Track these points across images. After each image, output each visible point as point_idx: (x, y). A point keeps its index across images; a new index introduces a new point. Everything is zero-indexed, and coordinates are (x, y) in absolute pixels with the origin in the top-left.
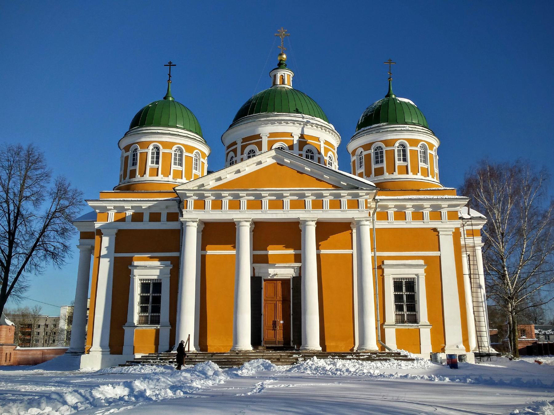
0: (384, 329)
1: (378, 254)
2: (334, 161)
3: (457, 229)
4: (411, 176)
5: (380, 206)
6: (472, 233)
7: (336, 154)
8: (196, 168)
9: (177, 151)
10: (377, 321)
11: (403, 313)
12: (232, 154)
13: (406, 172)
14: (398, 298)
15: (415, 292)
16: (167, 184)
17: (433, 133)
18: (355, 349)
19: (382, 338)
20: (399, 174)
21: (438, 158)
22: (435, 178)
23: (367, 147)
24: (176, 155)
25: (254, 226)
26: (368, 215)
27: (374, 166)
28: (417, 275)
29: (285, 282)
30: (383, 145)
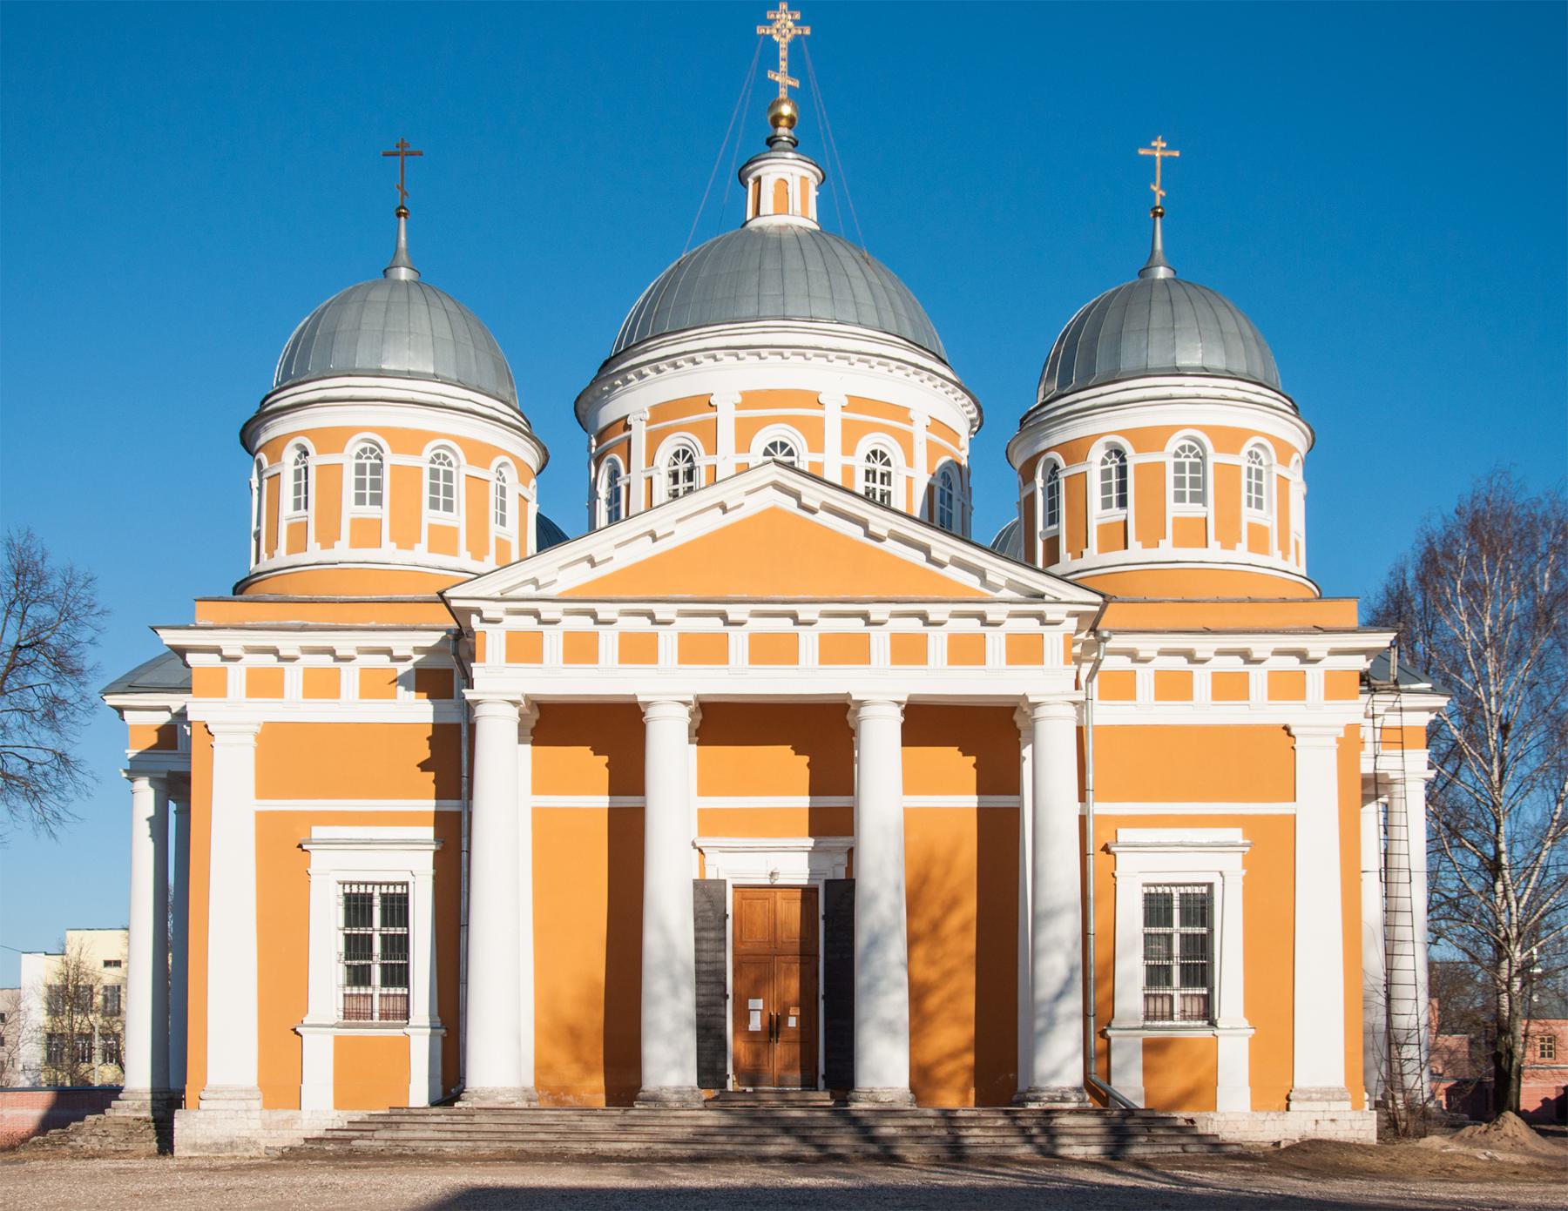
3: (1353, 729)
4: (1137, 552)
6: (1397, 739)
9: (438, 462)
17: (1294, 407)
20: (430, 550)
24: (1179, 468)
25: (700, 717)
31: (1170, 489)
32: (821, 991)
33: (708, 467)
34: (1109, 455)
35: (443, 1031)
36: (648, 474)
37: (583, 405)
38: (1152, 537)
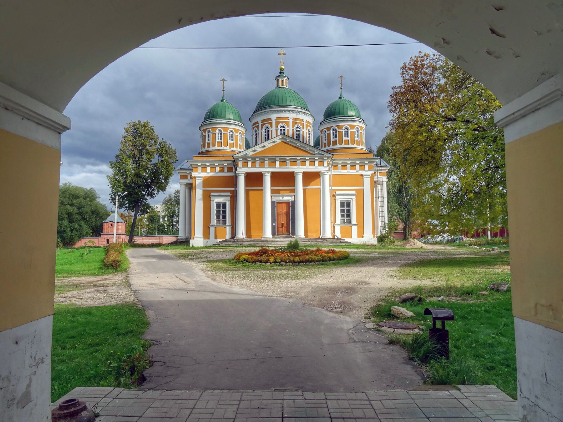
5: (335, 163)
6: (381, 174)
10: (331, 222)
11: (344, 218)
12: (256, 129)
14: (342, 211)
16: (226, 151)
18: (321, 236)
23: (329, 129)
24: (230, 134)
26: (328, 169)
28: (352, 199)
29: (287, 203)
30: (336, 128)
32: (290, 219)
38: (341, 143)
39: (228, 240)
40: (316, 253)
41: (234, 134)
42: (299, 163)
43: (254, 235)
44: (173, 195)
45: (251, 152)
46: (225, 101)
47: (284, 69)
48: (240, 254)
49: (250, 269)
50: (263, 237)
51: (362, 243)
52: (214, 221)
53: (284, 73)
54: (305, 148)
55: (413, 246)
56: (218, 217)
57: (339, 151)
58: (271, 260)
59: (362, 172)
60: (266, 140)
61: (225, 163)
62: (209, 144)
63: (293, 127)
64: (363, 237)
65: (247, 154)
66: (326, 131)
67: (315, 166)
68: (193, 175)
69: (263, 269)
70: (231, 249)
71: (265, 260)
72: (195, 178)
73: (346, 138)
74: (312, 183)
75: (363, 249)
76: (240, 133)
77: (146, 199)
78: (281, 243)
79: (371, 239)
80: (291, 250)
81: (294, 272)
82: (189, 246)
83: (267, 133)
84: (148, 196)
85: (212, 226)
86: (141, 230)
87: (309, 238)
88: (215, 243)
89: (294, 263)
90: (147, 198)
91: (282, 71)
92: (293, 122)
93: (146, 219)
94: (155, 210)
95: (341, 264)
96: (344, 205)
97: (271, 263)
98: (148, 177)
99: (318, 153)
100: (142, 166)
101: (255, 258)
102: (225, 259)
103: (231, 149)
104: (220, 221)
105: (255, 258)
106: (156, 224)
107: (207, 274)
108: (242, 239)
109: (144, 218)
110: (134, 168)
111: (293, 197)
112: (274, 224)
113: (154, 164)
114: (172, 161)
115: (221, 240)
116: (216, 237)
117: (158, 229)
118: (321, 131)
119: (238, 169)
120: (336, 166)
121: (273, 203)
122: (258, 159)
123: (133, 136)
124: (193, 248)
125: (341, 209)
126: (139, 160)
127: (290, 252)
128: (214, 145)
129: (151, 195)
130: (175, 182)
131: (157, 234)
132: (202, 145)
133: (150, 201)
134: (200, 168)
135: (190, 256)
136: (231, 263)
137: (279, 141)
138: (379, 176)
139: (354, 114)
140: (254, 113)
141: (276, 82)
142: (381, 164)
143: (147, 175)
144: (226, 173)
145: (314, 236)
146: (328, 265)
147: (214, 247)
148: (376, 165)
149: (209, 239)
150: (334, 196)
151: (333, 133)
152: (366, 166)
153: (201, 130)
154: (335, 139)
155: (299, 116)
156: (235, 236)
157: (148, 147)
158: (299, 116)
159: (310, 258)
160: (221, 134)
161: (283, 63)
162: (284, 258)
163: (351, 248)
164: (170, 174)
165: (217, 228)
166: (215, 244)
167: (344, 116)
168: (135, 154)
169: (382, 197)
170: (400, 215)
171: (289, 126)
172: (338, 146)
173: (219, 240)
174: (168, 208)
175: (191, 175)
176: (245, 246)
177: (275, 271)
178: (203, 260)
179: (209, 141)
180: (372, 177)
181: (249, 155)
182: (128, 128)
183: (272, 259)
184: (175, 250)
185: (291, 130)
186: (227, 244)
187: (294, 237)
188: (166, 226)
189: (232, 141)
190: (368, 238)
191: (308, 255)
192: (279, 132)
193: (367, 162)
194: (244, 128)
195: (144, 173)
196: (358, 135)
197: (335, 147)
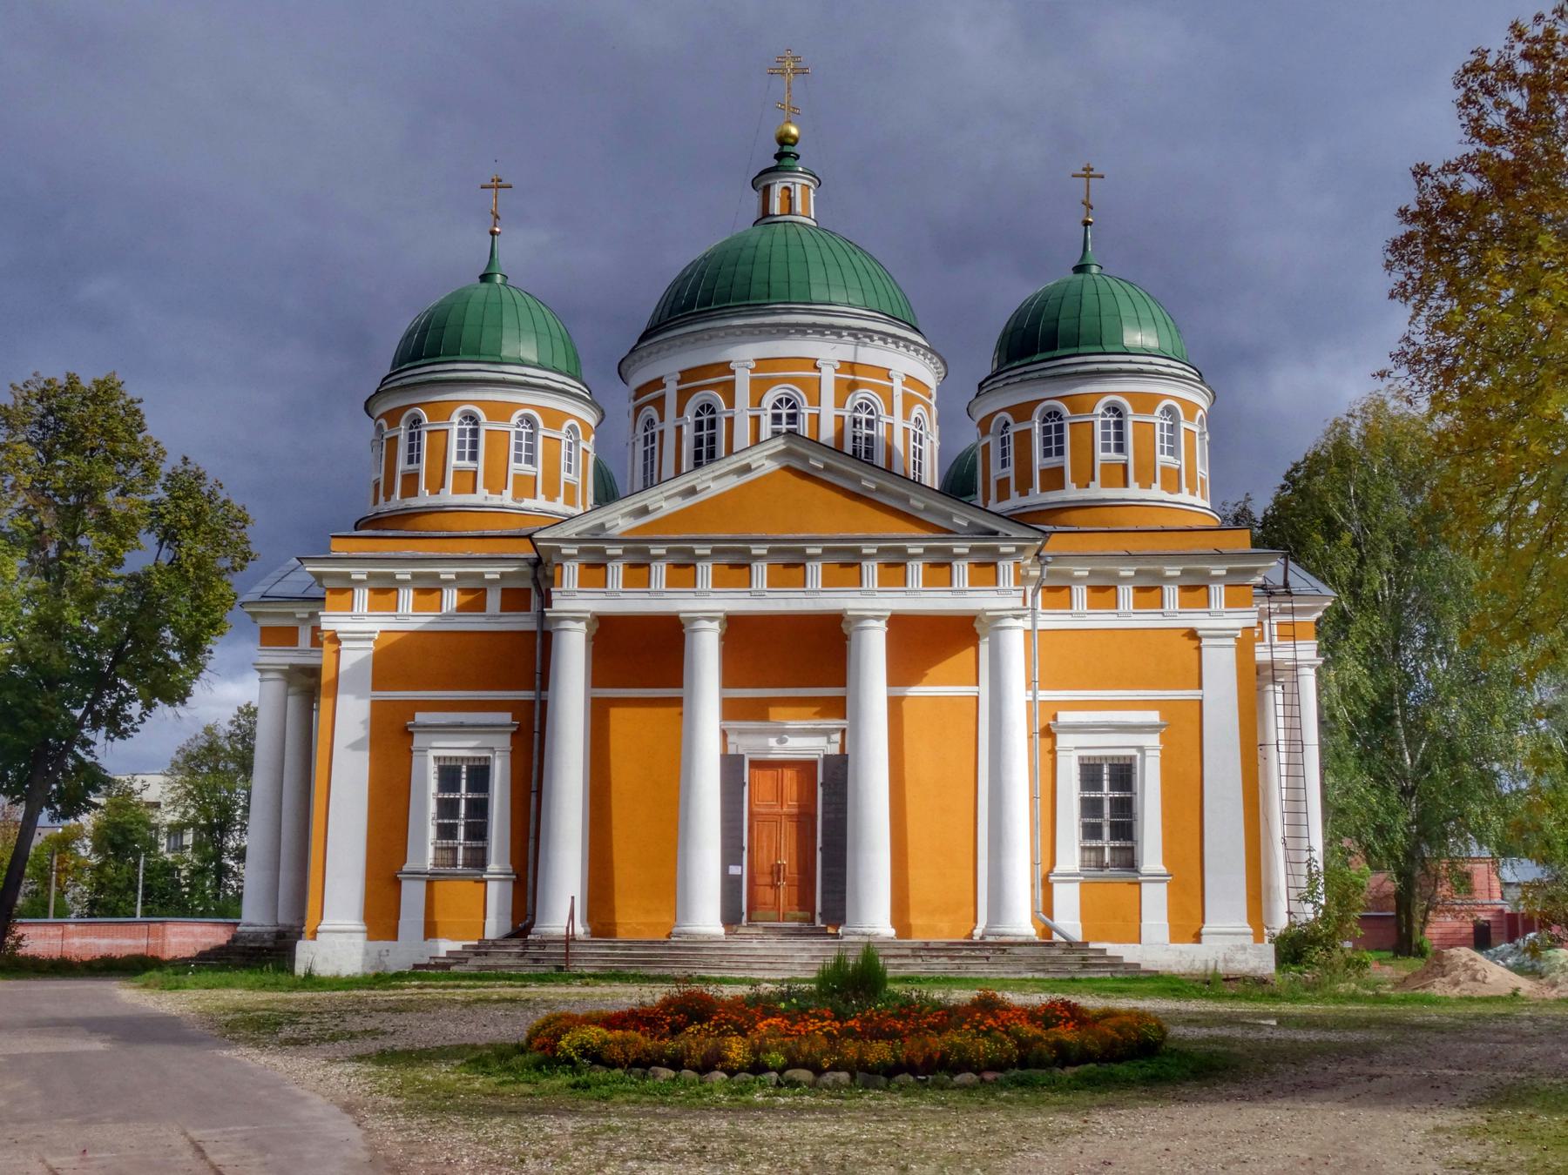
0: (1052, 884)
1: (1043, 695)
2: (928, 429)
6: (1290, 633)
7: (934, 408)
8: (570, 466)
10: (1034, 863)
12: (652, 412)
13: (1122, 484)
14: (1090, 807)
15: (1134, 791)
16: (501, 512)
18: (978, 932)
19: (1046, 906)
21: (1207, 437)
22: (1198, 493)
23: (1022, 412)
24: (519, 435)
26: (1019, 604)
27: (1038, 461)
28: (1141, 749)
29: (805, 767)
31: (512, 452)
32: (819, 844)
33: (727, 419)
34: (521, 422)
35: (514, 877)
36: (678, 424)
37: (624, 366)
38: (1084, 480)
39: (494, 943)
40: (981, 1023)
41: (541, 433)
42: (871, 570)
43: (632, 920)
44: (225, 728)
45: (624, 516)
46: (499, 279)
47: (796, 140)
48: (557, 1019)
49: (615, 1104)
50: (676, 930)
51: (1199, 966)
52: (425, 849)
53: (797, 157)
54: (905, 499)
55: (1467, 988)
56: (446, 832)
57: (1074, 514)
58: (732, 1055)
59: (1198, 620)
60: (698, 465)
61: (492, 572)
62: (411, 481)
63: (840, 404)
64: (1197, 938)
65: (602, 525)
66: (1010, 420)
67: (955, 586)
68: (324, 627)
69: (690, 1108)
70: (509, 992)
71: (697, 1055)
72: (335, 639)
73: (1113, 455)
74: (933, 672)
75: (1207, 997)
76: (572, 427)
77: (86, 743)
78: (771, 962)
79: (1244, 948)
80: (842, 1006)
81: (872, 1130)
82: (292, 971)
83: (705, 433)
84: (95, 727)
85: (416, 875)
86: (62, 893)
87: (917, 939)
88: (425, 961)
89: (859, 1075)
90: (91, 736)
91: (787, 149)
92: (837, 380)
93: (87, 842)
94: (136, 799)
95: (1127, 1084)
96: (1100, 780)
97: (731, 1073)
98: (101, 636)
99: (971, 523)
100: (74, 583)
101: (643, 1041)
102: (474, 1047)
103: (523, 505)
104: (455, 850)
105: (643, 1041)
106: (137, 865)
107: (370, 1131)
108: (569, 940)
109: (77, 834)
110: (36, 592)
111: (837, 737)
112: (734, 870)
113: (133, 578)
114: (226, 563)
115: (456, 946)
116: (431, 931)
117: (144, 886)
118: (984, 425)
119: (554, 596)
120: (1063, 588)
121: (731, 765)
122: (656, 550)
123: (36, 445)
124: (311, 981)
125: (1084, 801)
126: (60, 556)
127: (839, 1016)
128: (437, 485)
129: (115, 724)
130: (235, 672)
131: (139, 913)
132: (377, 486)
133: (106, 751)
134: (362, 596)
135: (291, 1022)
136: (510, 1069)
137: (771, 466)
138: (1276, 641)
139: (1151, 342)
140: (645, 336)
141: (755, 198)
142: (1286, 585)
143: (96, 629)
144: (494, 619)
145: (943, 930)
146: (1053, 1086)
147: (419, 977)
148: (1263, 587)
149: (396, 938)
150: (1048, 733)
151: (1047, 430)
152: (1218, 592)
153: (377, 415)
154: (1054, 461)
155: (872, 354)
156: (532, 924)
157: (109, 497)
158: (872, 354)
159: (953, 1046)
160: (475, 433)
161: (793, 114)
162: (805, 1048)
163: (1143, 995)
164: (213, 625)
165: (438, 886)
166: (426, 966)
167: (1100, 349)
168: (40, 528)
169: (1295, 744)
170: (1381, 831)
171: (816, 400)
172: (1072, 493)
173: (445, 946)
174: (199, 787)
175: (316, 629)
176: (581, 977)
177: (758, 1120)
178: (358, 1047)
179: (411, 467)
180: (1245, 643)
181: (615, 533)
182: (15, 406)
183: (737, 1050)
184: (215, 992)
185: (827, 417)
186: (489, 967)
187: (836, 936)
188: (184, 873)
189: (529, 467)
190: (1228, 942)
191: (940, 1029)
192: (766, 427)
193: (1219, 570)
194: (593, 404)
195: (82, 618)
196: (1170, 440)
197: (1054, 497)
